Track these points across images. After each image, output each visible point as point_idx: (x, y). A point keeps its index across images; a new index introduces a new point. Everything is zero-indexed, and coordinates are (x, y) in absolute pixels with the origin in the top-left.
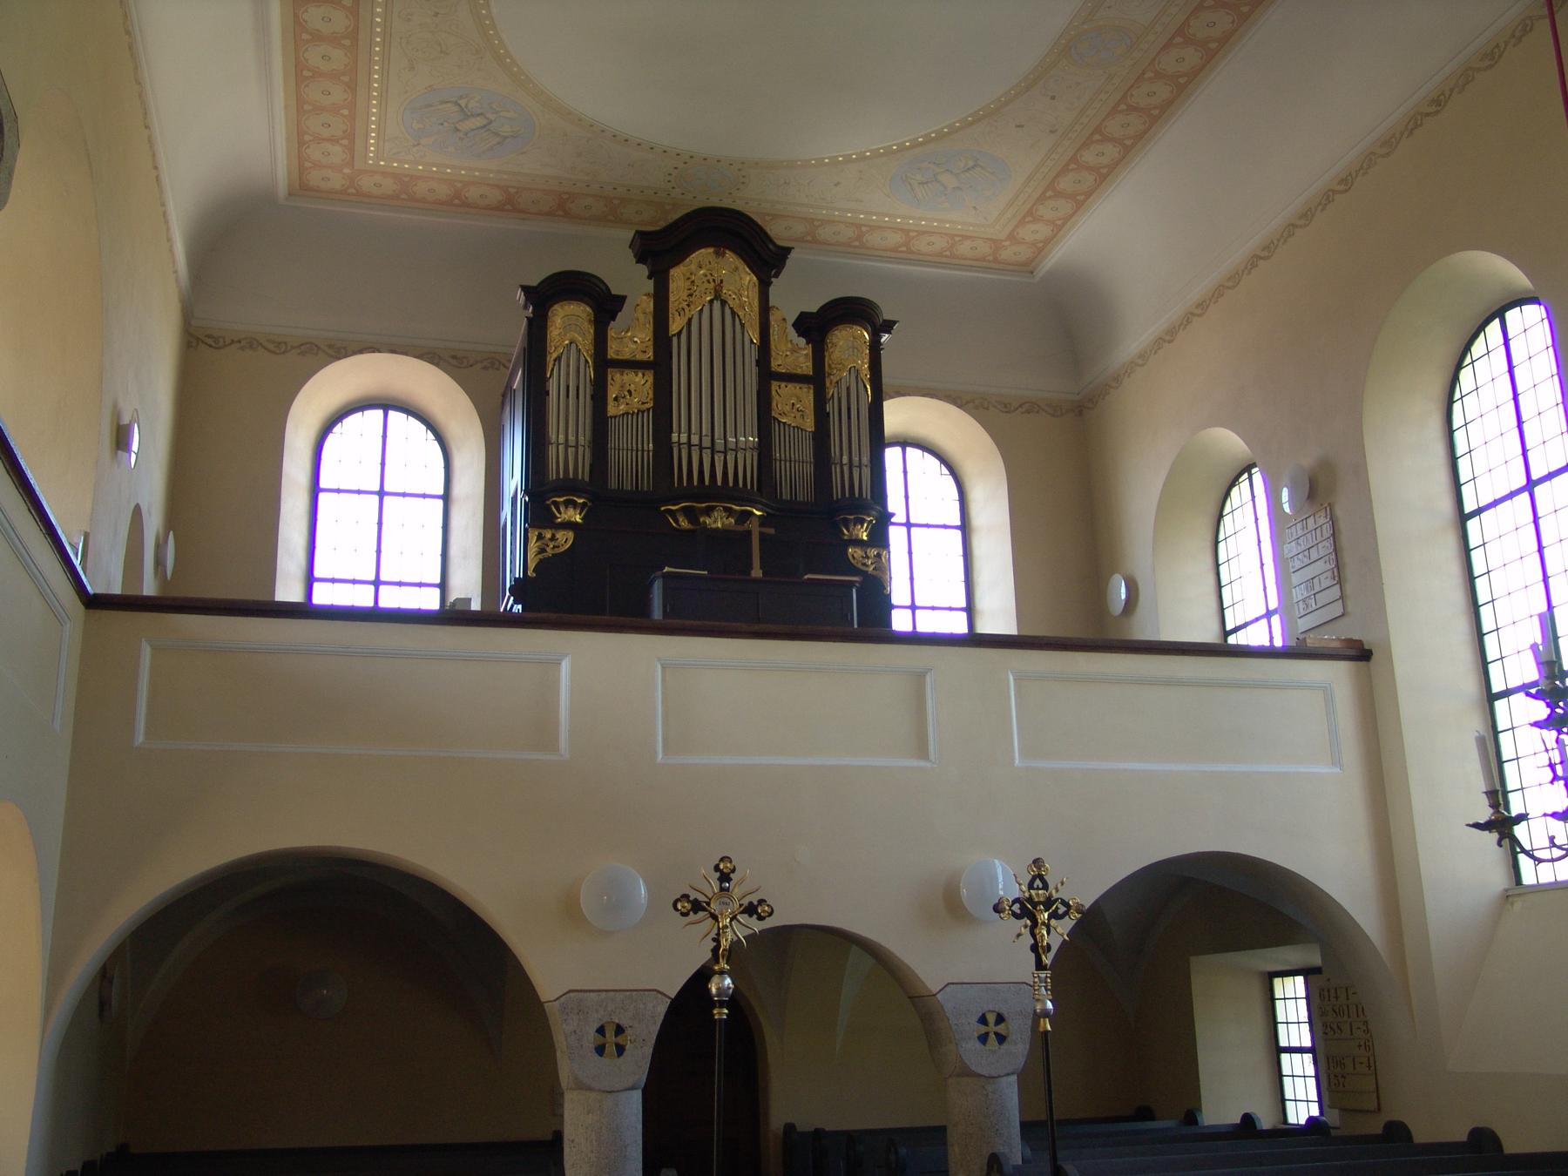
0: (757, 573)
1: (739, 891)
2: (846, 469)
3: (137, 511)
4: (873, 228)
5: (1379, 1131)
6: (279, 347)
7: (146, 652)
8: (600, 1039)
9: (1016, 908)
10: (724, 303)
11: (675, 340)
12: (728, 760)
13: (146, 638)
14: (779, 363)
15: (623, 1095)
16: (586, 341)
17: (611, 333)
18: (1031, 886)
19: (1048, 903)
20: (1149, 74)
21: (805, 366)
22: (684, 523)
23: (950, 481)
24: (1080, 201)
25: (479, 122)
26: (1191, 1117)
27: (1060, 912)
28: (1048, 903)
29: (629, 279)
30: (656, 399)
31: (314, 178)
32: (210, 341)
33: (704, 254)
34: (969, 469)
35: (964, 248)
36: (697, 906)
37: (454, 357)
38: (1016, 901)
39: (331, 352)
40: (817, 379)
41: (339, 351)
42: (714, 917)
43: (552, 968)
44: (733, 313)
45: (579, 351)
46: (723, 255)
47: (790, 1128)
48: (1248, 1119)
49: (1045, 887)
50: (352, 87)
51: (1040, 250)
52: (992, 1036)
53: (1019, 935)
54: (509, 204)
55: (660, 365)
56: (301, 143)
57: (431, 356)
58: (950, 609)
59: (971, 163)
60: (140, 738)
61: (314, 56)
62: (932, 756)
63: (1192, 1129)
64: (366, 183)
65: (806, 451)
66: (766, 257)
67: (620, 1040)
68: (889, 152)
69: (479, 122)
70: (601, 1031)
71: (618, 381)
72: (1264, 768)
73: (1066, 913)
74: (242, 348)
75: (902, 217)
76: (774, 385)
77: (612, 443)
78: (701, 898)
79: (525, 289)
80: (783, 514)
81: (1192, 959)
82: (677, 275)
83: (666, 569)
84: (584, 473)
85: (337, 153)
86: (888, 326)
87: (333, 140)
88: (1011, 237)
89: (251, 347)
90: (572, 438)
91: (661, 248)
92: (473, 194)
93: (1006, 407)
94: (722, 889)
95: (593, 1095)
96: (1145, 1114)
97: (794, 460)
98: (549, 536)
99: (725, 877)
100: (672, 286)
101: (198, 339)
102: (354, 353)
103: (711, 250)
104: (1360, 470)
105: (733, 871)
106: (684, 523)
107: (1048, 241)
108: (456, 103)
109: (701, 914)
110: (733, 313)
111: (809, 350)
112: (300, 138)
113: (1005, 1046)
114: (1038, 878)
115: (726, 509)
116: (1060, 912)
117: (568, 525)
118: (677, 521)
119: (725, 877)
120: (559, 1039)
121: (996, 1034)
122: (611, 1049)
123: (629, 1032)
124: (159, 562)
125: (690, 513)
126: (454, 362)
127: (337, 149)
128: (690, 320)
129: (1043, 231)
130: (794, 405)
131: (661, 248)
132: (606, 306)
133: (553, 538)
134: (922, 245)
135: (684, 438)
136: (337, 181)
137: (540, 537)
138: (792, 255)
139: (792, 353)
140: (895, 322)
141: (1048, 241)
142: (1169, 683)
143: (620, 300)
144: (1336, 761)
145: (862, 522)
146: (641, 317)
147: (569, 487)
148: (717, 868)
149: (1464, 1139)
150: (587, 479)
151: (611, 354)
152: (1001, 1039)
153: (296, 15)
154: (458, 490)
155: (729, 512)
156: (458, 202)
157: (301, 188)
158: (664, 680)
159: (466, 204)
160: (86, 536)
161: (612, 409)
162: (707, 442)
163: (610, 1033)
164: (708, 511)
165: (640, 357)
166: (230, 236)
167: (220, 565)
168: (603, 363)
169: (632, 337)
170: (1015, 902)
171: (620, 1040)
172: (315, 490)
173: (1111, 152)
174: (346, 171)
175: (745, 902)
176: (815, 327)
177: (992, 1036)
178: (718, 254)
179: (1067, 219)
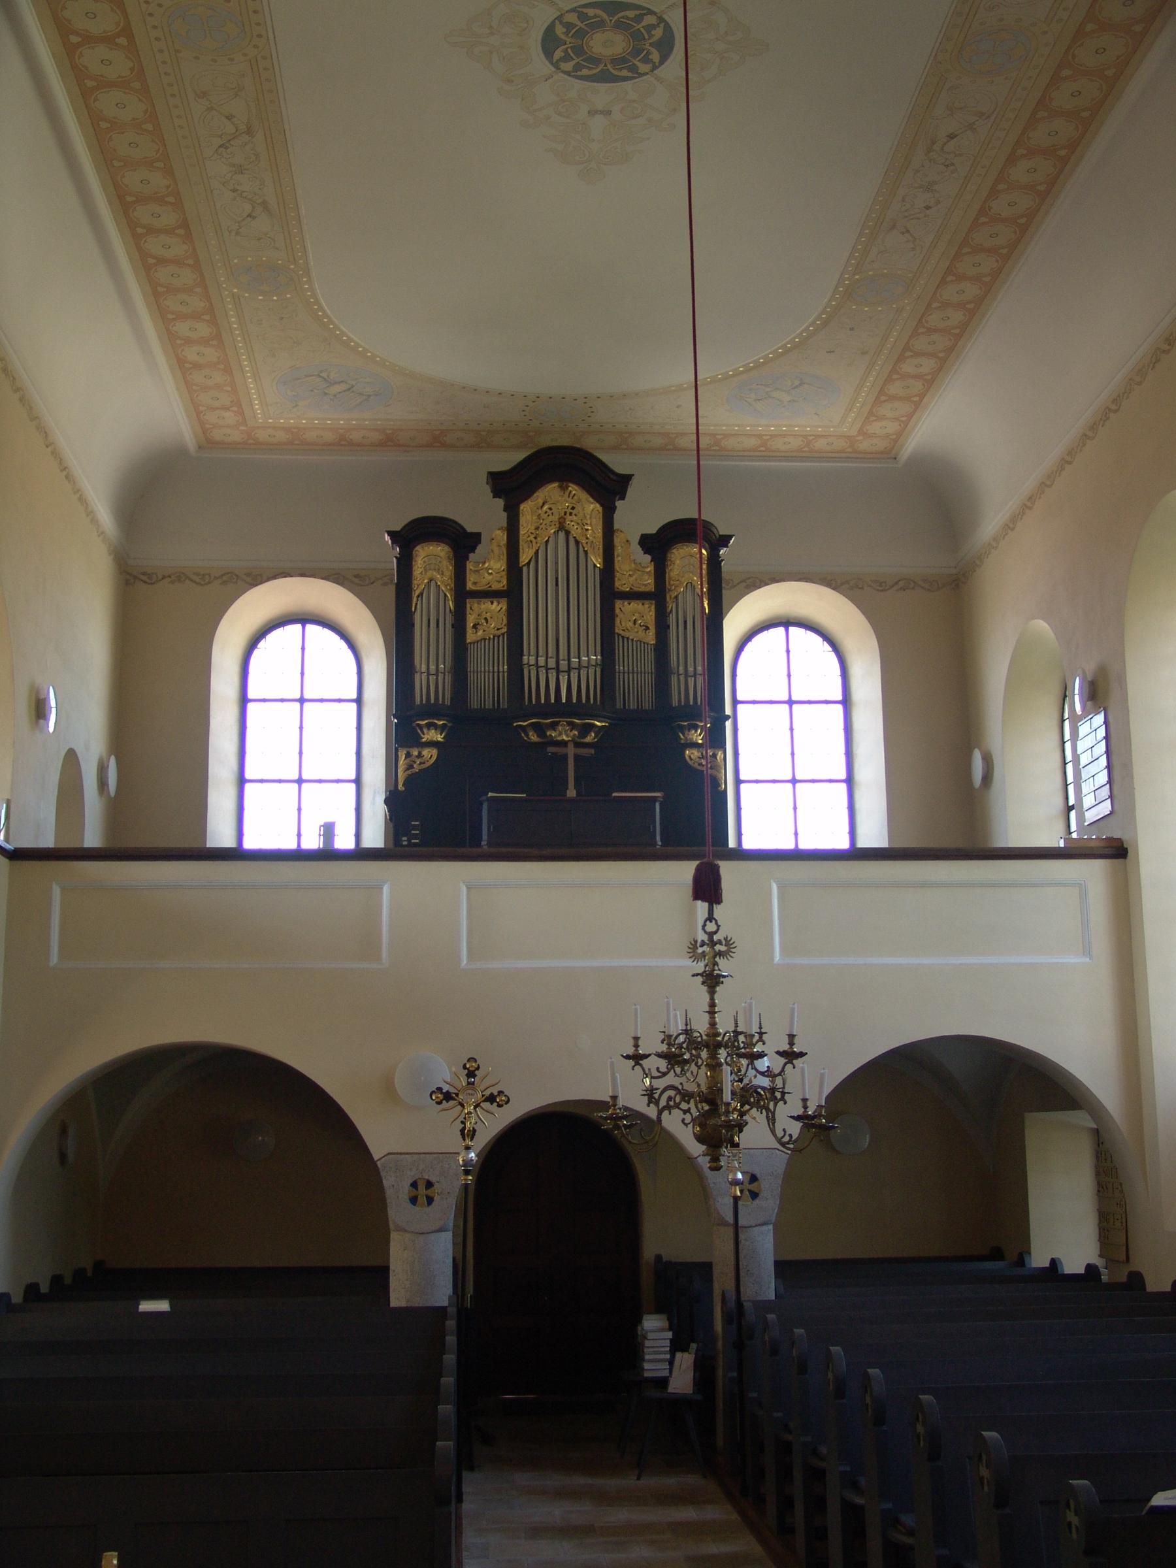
0: (571, 793)
1: (484, 1084)
2: (682, 678)
3: (71, 757)
4: (726, 436)
5: (1124, 1279)
6: (203, 578)
7: (57, 892)
8: (414, 1192)
10: (567, 533)
11: (525, 569)
12: (520, 964)
13: (56, 886)
14: (623, 583)
15: (433, 1237)
16: (444, 577)
17: (470, 566)
19: (677, 1106)
20: (935, 305)
21: (648, 583)
22: (534, 737)
23: (833, 656)
24: (917, 402)
25: (343, 387)
26: (1021, 1261)
29: (482, 513)
30: (509, 624)
31: (217, 435)
32: (144, 578)
33: (550, 491)
34: (849, 645)
35: (820, 444)
36: (448, 1097)
37: (357, 576)
39: (248, 579)
40: (658, 595)
41: (256, 578)
42: (462, 1105)
43: (382, 1134)
44: (577, 542)
45: (438, 587)
46: (567, 487)
47: (659, 1258)
50: (228, 371)
51: (896, 441)
54: (389, 441)
55: (513, 593)
56: (198, 413)
57: (337, 577)
58: (831, 781)
59: (797, 383)
60: (54, 959)
61: (191, 354)
64: (262, 435)
65: (646, 663)
66: (609, 487)
67: (429, 1192)
68: (726, 377)
69: (343, 387)
70: (414, 1185)
71: (476, 610)
72: (1012, 959)
74: (172, 582)
75: (750, 425)
76: (618, 604)
77: (471, 667)
78: (452, 1090)
79: (390, 533)
80: (626, 722)
81: (1026, 1114)
82: (526, 508)
83: (490, 794)
84: (446, 697)
85: (230, 417)
86: (724, 540)
87: (226, 408)
88: (861, 432)
89: (179, 581)
90: (433, 668)
91: (512, 487)
92: (356, 436)
93: (881, 585)
94: (469, 1083)
96: (996, 1254)
97: (635, 673)
98: (416, 753)
99: (471, 1074)
100: (522, 520)
101: (135, 578)
102: (268, 580)
103: (556, 485)
104: (1122, 679)
105: (478, 1068)
106: (534, 737)
107: (899, 434)
108: (319, 376)
109: (452, 1103)
110: (577, 542)
111: (651, 568)
112: (196, 411)
113: (757, 1202)
115: (569, 724)
117: (432, 744)
118: (527, 735)
120: (389, 1192)
122: (422, 1200)
123: (436, 1186)
124: (102, 784)
125: (539, 729)
126: (357, 581)
127: (227, 414)
128: (537, 553)
129: (891, 427)
130: (635, 619)
131: (512, 487)
132: (463, 543)
133: (420, 756)
134: (778, 444)
135: (532, 660)
136: (236, 436)
137: (408, 755)
138: (634, 483)
139: (635, 569)
140: (730, 537)
141: (899, 434)
142: (924, 885)
143: (476, 538)
144: (1087, 951)
145: (696, 727)
146: (496, 550)
147: (432, 711)
149: (1168, 1289)
150: (448, 702)
151: (470, 586)
153: (168, 330)
154: (368, 695)
155: (573, 726)
156: (343, 443)
157: (208, 443)
158: (468, 899)
159: (351, 444)
160: (8, 803)
161: (471, 636)
162: (552, 663)
163: (421, 1187)
164: (553, 726)
165: (496, 586)
166: (154, 487)
167: (152, 787)
168: (462, 594)
169: (488, 568)
171: (429, 1192)
172: (244, 700)
173: (928, 365)
174: (242, 428)
175: (487, 1093)
176: (658, 545)
178: (563, 488)
179: (910, 416)
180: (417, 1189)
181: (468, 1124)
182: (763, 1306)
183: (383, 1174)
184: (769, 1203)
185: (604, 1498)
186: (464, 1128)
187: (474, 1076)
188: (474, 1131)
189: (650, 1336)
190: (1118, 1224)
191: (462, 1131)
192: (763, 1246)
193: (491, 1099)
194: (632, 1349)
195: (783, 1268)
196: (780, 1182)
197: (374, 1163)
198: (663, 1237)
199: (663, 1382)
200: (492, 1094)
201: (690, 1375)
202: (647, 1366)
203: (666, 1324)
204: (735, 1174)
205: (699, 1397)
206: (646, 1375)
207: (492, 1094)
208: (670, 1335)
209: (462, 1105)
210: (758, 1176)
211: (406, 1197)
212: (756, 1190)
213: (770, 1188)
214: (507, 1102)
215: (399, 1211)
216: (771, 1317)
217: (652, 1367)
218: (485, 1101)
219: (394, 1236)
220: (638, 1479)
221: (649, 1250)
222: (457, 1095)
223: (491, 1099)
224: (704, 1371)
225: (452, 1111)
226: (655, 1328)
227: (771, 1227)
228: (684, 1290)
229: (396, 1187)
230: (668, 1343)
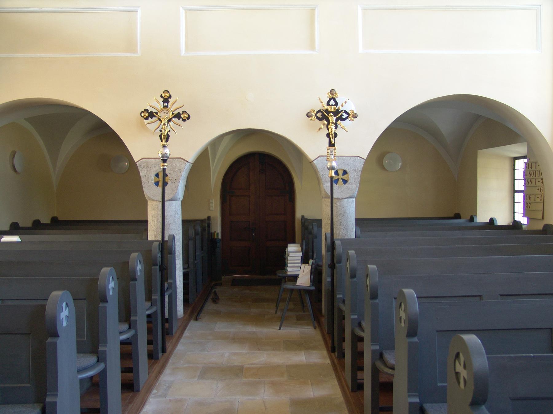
1: (173, 107)
9: (319, 115)
18: (328, 104)
19: (336, 113)
26: (472, 219)
27: (344, 117)
28: (336, 113)
38: (319, 111)
42: (160, 120)
47: (303, 217)
48: (492, 220)
49: (336, 104)
52: (341, 180)
53: (320, 129)
62: (317, 50)
63: (472, 224)
73: (347, 118)
94: (164, 106)
95: (155, 202)
96: (457, 216)
99: (166, 101)
105: (170, 97)
109: (154, 119)
113: (346, 185)
114: (333, 98)
116: (344, 117)
119: (166, 101)
120: (143, 179)
121: (342, 179)
148: (161, 96)
152: (345, 182)
170: (318, 112)
175: (176, 112)
177: (341, 180)
180: (159, 178)
181: (163, 131)
182: (347, 242)
183: (140, 169)
184: (353, 186)
185: (257, 343)
186: (162, 134)
187: (168, 102)
188: (168, 136)
189: (291, 254)
190: (538, 200)
191: (161, 136)
192: (349, 210)
193: (178, 116)
194: (281, 261)
195: (359, 222)
196: (359, 174)
197: (135, 163)
198: (305, 207)
199: (295, 278)
200: (179, 113)
201: (308, 276)
202: (289, 269)
203: (300, 249)
204: (332, 163)
205: (313, 288)
206: (289, 273)
207: (179, 113)
208: (301, 254)
209: (160, 120)
210: (347, 171)
211: (153, 182)
212: (346, 179)
213: (354, 177)
214: (189, 118)
215: (151, 191)
216: (352, 252)
217: (291, 270)
218: (174, 117)
219: (149, 203)
220: (280, 329)
221: (299, 214)
222: (157, 113)
223: (178, 116)
224: (316, 274)
225: (152, 125)
226: (294, 251)
227: (354, 199)
228: (309, 233)
229: (147, 177)
230: (300, 258)
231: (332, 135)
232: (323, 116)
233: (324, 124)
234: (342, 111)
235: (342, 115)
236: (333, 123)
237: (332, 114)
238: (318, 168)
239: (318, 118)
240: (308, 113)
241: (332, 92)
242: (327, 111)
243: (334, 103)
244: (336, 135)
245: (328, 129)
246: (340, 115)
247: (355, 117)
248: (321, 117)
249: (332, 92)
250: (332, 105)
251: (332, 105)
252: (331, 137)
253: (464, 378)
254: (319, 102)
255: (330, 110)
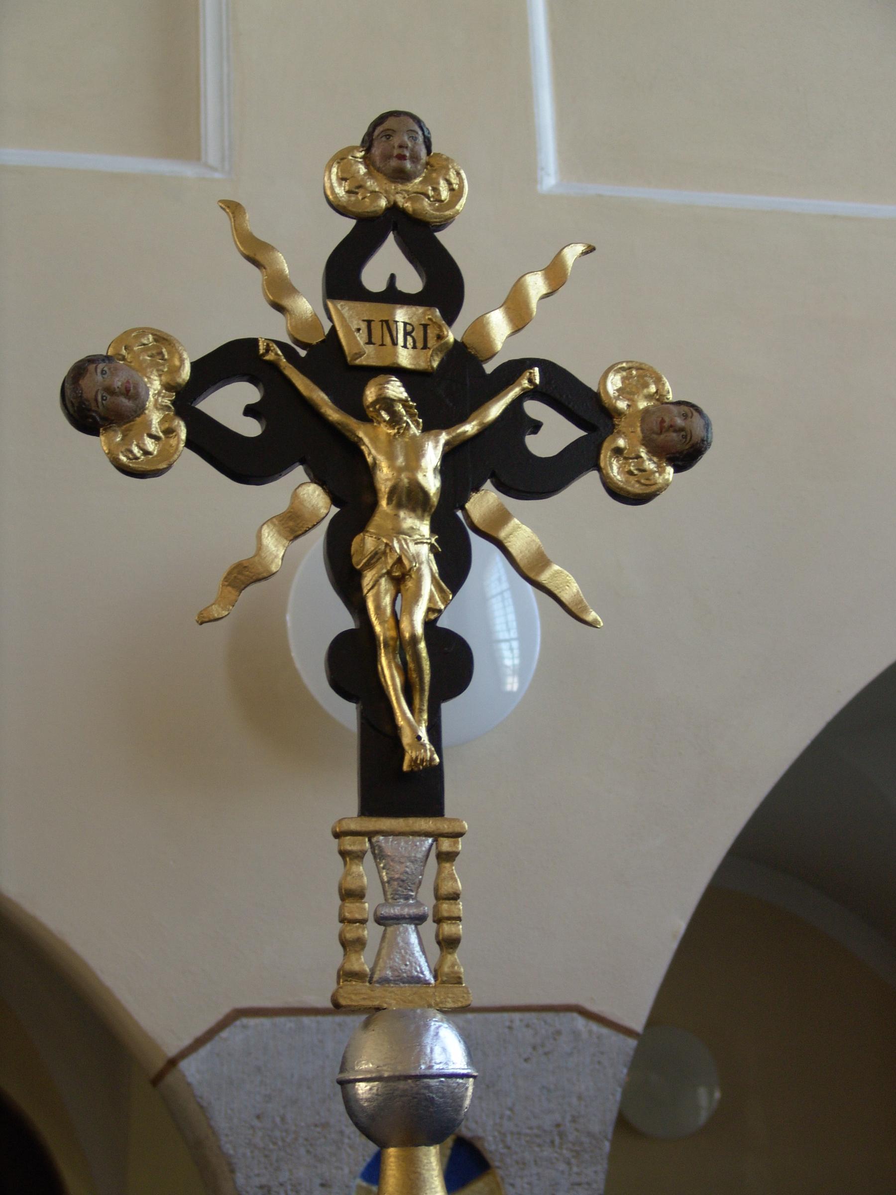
9: (231, 405)
18: (342, 276)
19: (452, 384)
38: (234, 360)
49: (444, 287)
73: (579, 460)
231: (403, 647)
232: (291, 416)
233: (293, 525)
234: (513, 370)
235: (516, 422)
236: (412, 497)
237: (396, 389)
238: (221, 1123)
239: (210, 441)
240: (79, 371)
241: (393, 142)
242: (326, 358)
243: (411, 281)
244: (451, 662)
245: (346, 580)
246: (495, 410)
247: (685, 454)
248: (251, 428)
249: (393, 142)
250: (392, 295)
251: (392, 295)
252: (390, 676)
253: (72, 402)
254: (224, 251)
255: (370, 357)
